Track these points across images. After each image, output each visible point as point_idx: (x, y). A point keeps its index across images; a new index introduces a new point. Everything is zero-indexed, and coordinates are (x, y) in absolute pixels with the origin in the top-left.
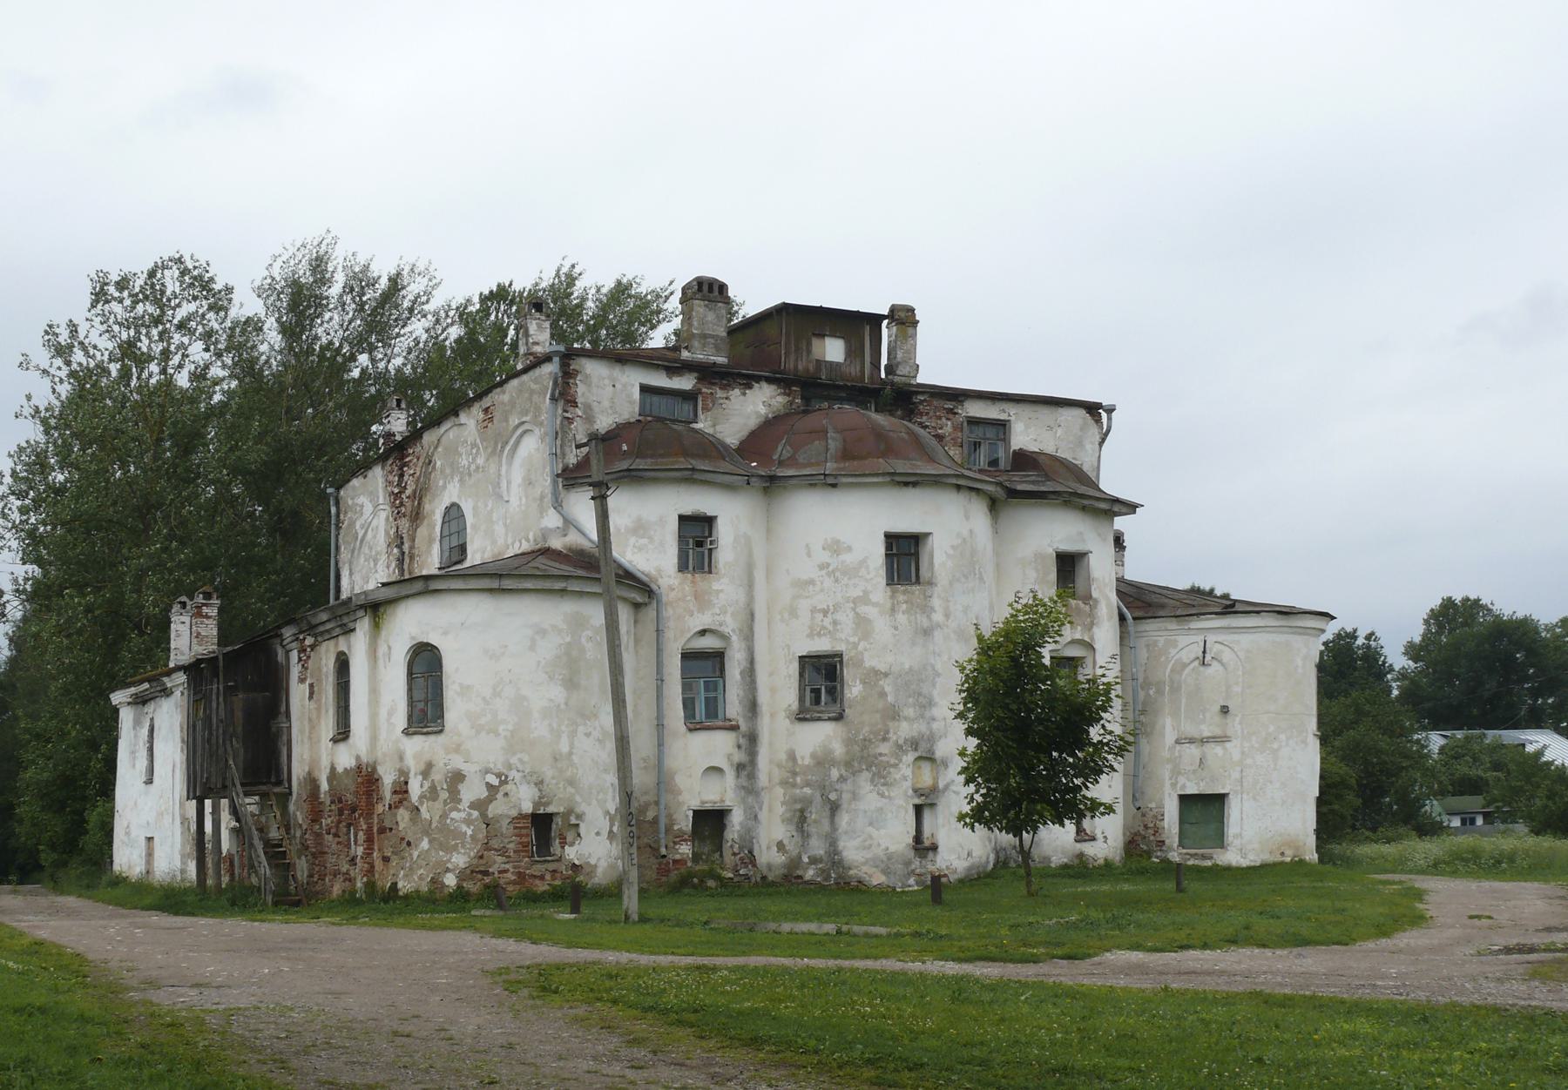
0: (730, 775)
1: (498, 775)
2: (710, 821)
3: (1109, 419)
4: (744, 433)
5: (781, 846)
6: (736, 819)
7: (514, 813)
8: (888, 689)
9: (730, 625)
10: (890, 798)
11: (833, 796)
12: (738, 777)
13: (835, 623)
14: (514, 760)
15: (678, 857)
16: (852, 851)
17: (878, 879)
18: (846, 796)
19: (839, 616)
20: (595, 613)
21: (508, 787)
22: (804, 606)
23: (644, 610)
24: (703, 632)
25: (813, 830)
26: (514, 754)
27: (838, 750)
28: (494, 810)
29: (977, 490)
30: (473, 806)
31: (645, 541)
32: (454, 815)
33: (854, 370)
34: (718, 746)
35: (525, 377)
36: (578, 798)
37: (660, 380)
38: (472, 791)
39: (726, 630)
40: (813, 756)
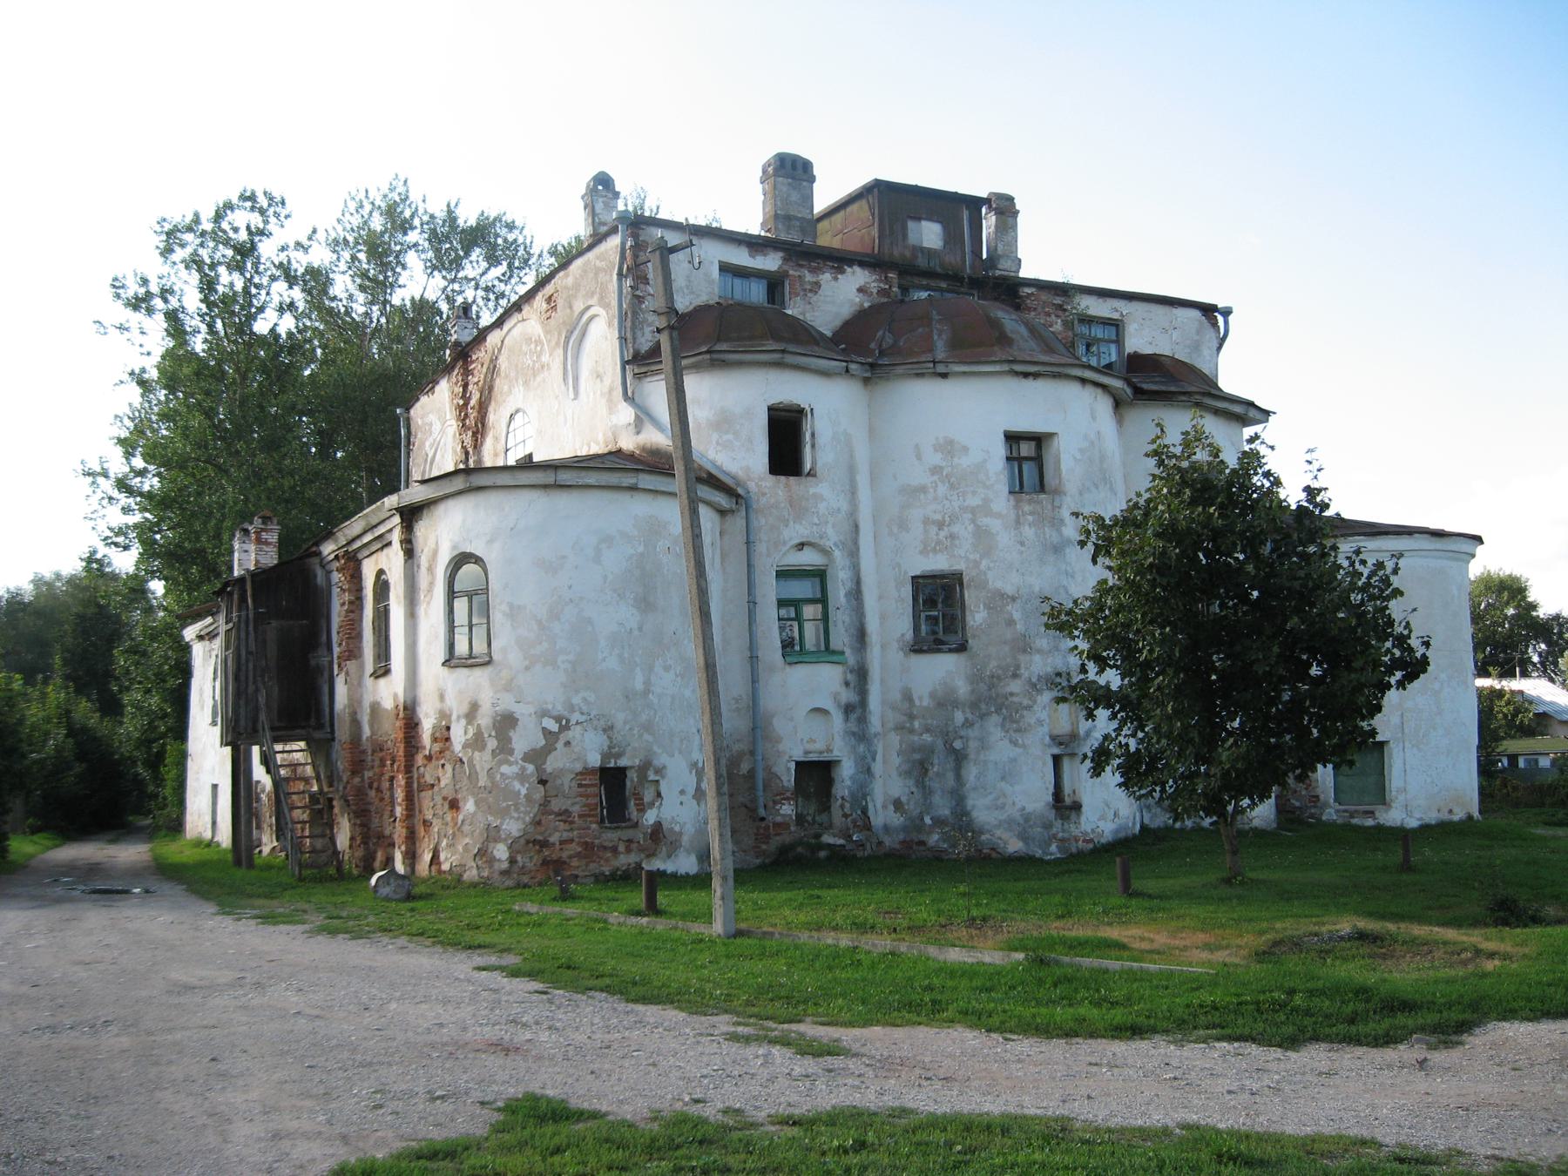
0: (837, 718)
1: (558, 719)
2: (816, 775)
3: (1226, 323)
4: (838, 323)
5: (898, 805)
6: (846, 772)
7: (579, 767)
8: (1017, 616)
9: (832, 536)
10: (1024, 746)
11: (958, 744)
12: (847, 720)
13: (952, 536)
14: (576, 700)
15: (779, 819)
16: (982, 811)
17: (1014, 846)
18: (973, 745)
19: (955, 529)
20: (671, 513)
21: (569, 735)
22: (916, 515)
23: (729, 518)
24: (801, 546)
25: (935, 785)
26: (577, 692)
27: (963, 689)
28: (553, 763)
29: (1104, 387)
30: (527, 758)
31: (730, 436)
32: (505, 769)
33: (951, 259)
34: (821, 683)
35: (590, 255)
36: (655, 748)
37: (741, 257)
38: (525, 739)
39: (829, 544)
40: (932, 695)
